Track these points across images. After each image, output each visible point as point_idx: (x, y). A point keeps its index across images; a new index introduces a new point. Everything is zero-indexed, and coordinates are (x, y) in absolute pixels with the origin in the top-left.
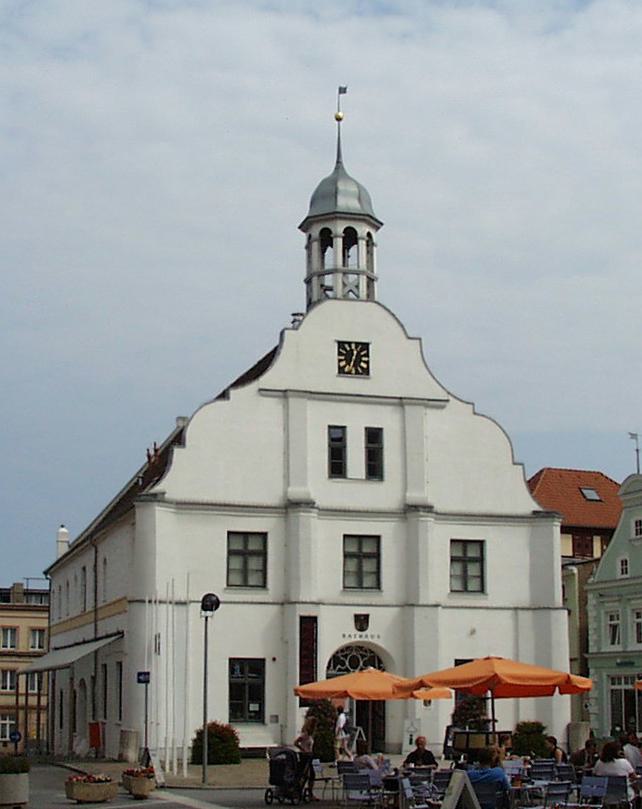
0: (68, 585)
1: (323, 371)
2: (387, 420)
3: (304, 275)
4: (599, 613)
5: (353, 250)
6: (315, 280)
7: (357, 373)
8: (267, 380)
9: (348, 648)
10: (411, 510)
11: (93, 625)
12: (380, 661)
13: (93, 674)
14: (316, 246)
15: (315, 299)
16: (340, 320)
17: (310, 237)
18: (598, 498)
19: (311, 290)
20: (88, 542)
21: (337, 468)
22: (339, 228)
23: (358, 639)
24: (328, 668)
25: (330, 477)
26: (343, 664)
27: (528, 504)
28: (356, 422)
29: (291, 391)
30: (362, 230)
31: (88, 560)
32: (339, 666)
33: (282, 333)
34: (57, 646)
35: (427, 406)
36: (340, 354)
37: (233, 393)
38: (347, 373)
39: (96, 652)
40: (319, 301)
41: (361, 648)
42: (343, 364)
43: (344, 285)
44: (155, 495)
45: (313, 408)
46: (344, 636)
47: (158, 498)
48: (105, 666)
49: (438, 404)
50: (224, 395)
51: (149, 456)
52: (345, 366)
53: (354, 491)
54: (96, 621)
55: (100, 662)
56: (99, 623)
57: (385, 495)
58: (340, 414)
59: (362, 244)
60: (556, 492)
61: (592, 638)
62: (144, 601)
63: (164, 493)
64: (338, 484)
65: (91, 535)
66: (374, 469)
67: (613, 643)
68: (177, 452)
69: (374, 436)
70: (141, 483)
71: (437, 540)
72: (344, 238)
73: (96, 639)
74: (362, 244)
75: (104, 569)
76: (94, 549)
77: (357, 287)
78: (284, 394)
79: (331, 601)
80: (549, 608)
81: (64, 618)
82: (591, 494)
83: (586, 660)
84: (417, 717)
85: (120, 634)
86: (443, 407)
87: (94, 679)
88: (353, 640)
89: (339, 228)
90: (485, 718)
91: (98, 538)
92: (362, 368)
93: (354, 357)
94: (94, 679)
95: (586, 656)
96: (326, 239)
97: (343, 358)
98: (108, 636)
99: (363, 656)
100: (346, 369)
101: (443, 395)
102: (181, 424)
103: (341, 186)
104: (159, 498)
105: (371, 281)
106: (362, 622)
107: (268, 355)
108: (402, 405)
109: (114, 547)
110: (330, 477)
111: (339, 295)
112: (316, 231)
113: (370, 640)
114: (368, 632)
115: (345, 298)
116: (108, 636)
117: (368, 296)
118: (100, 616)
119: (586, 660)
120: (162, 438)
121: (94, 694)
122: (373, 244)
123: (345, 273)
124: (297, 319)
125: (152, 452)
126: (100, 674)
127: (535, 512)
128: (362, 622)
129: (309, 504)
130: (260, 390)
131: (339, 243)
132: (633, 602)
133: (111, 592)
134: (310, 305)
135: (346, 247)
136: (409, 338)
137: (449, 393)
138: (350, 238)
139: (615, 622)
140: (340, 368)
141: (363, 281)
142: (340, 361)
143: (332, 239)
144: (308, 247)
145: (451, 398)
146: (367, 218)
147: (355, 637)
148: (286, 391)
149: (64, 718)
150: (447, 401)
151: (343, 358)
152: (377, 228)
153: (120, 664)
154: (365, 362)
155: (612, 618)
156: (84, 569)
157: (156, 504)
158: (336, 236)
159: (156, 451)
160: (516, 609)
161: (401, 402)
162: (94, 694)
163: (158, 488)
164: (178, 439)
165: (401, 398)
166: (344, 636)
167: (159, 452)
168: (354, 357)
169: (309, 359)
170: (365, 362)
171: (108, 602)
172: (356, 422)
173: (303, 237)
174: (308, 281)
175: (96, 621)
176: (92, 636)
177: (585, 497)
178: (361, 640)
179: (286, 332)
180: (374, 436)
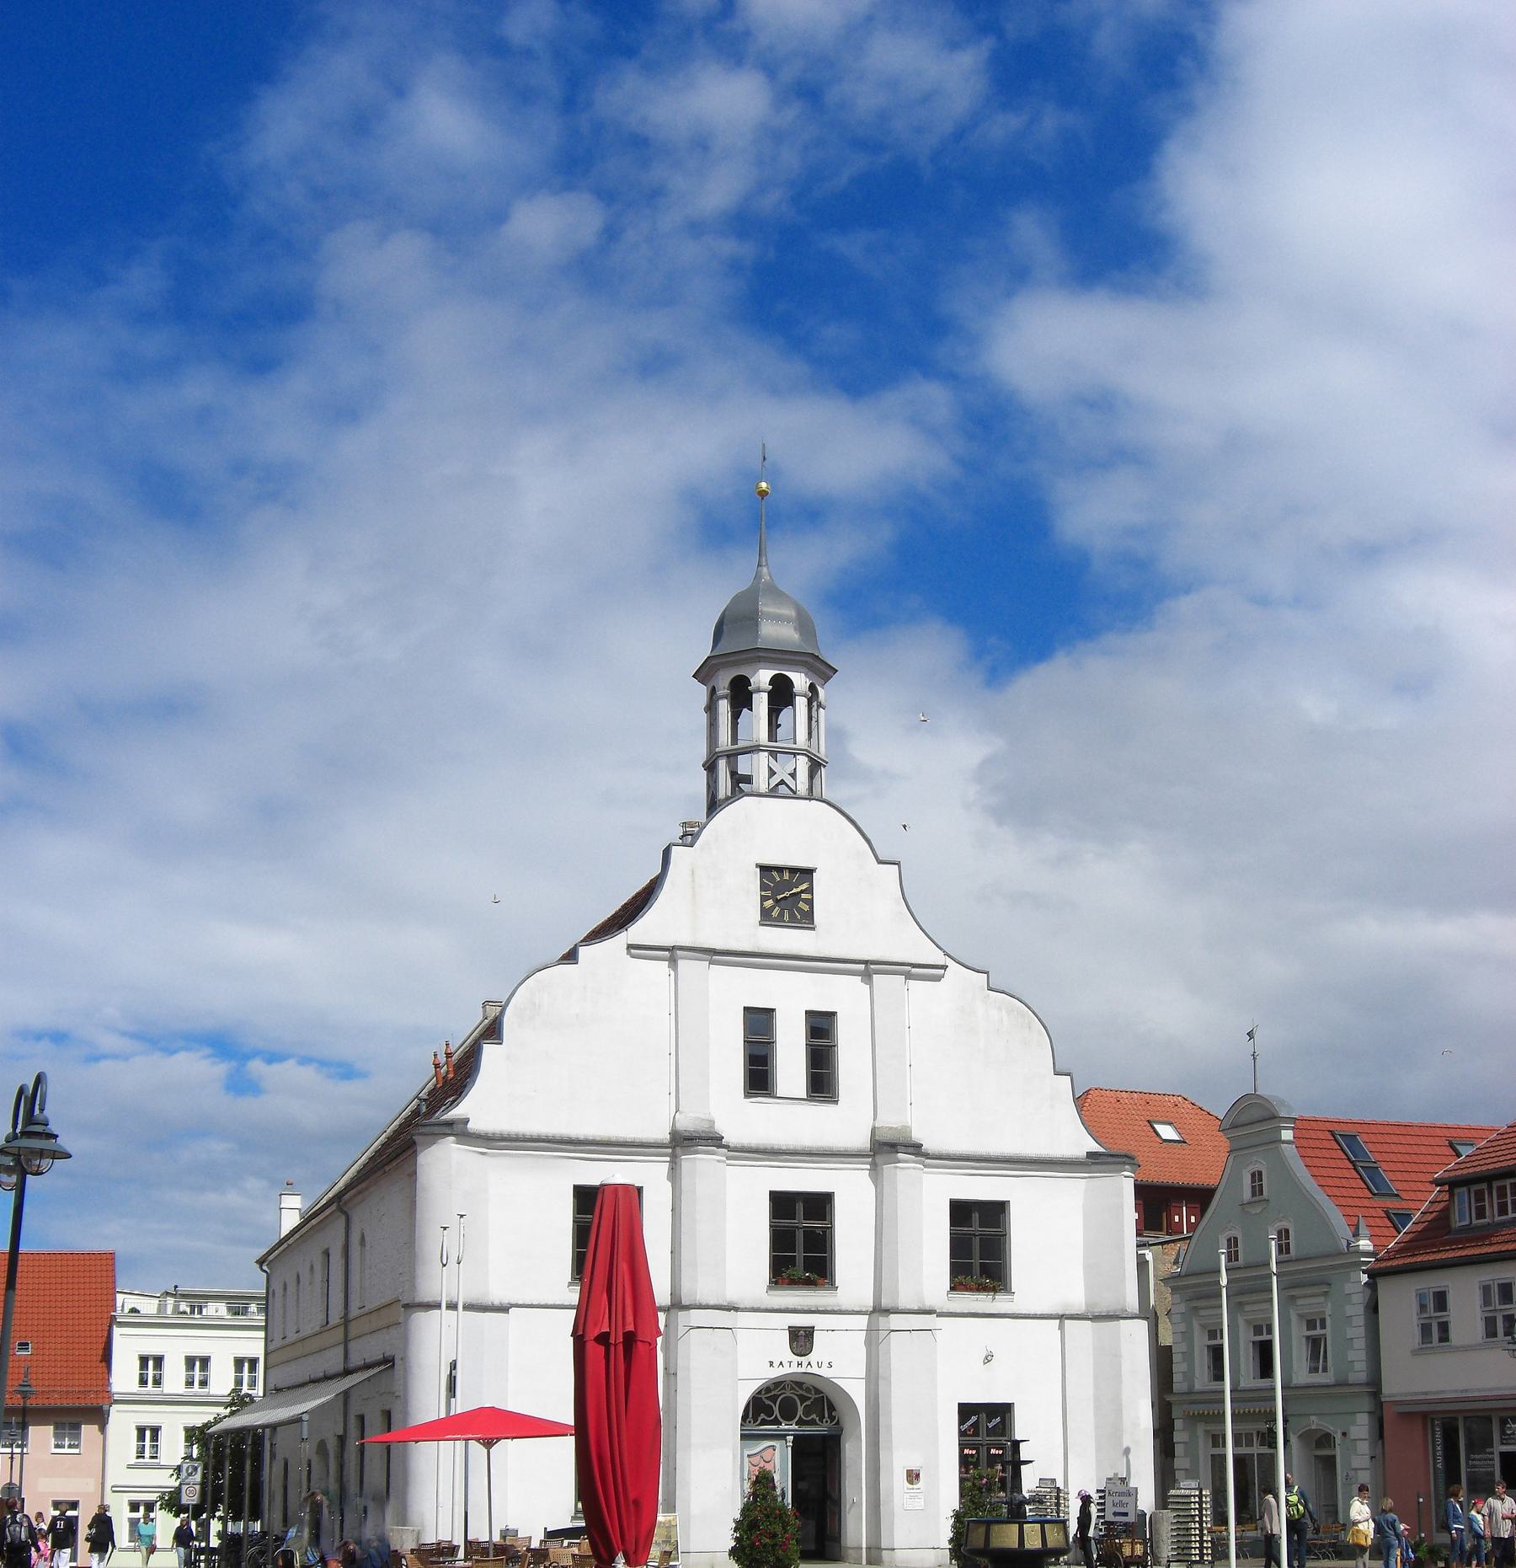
0: (285, 1289)
1: (736, 916)
2: (840, 995)
3: (701, 752)
5: (785, 715)
6: (722, 764)
7: (793, 918)
8: (638, 931)
9: (778, 1384)
10: (887, 1148)
11: (341, 1348)
12: (832, 1408)
13: (341, 1433)
14: (724, 707)
15: (721, 795)
16: (766, 829)
17: (713, 691)
18: (1177, 1138)
19: (716, 781)
20: (334, 1207)
21: (759, 1078)
22: (763, 677)
23: (795, 1369)
24: (744, 1418)
25: (748, 1095)
26: (770, 1412)
27: (1081, 1143)
28: (792, 1000)
29: (682, 948)
30: (800, 681)
31: (333, 1237)
32: (763, 1416)
34: (280, 1386)
35: (909, 976)
36: (763, 887)
38: (775, 920)
39: (346, 1394)
40: (729, 800)
41: (799, 1384)
42: (769, 903)
43: (772, 773)
44: (450, 1124)
45: (721, 975)
46: (771, 1364)
47: (459, 1131)
48: (361, 1418)
49: (929, 972)
50: (571, 957)
51: (437, 1066)
52: (772, 908)
53: (788, 1118)
54: (346, 1341)
55: (354, 1411)
56: (352, 1345)
57: (845, 1122)
58: (762, 988)
59: (801, 703)
60: (1115, 1124)
61: (1178, 1368)
62: (438, 1306)
63: (467, 1121)
64: (760, 1107)
65: (339, 1196)
66: (822, 1081)
67: (1314, 1370)
68: (489, 1051)
69: (820, 1027)
70: (424, 1109)
71: (929, 1198)
72: (770, 693)
73: (347, 1372)
74: (801, 703)
76: (342, 1221)
77: (793, 775)
78: (672, 954)
79: (748, 1306)
80: (1096, 1318)
81: (292, 1337)
82: (1167, 1132)
83: (1169, 1404)
84: (1029, 1481)
86: (938, 979)
87: (342, 1440)
88: (786, 1370)
89: (763, 677)
91: (351, 1199)
92: (800, 910)
93: (786, 892)
94: (342, 1440)
95: (1169, 1398)
96: (741, 696)
97: (769, 893)
98: (367, 1367)
99: (803, 1399)
100: (775, 913)
102: (493, 1012)
105: (815, 766)
106: (801, 1340)
107: (638, 895)
108: (867, 976)
109: (370, 1216)
110: (748, 1095)
111: (763, 788)
112: (723, 681)
113: (815, 1370)
114: (813, 1357)
115: (773, 793)
116: (367, 1367)
118: (352, 1334)
119: (1169, 1404)
120: (462, 1028)
121: (341, 1466)
122: (820, 705)
123: (773, 754)
124: (690, 836)
125: (442, 1059)
126: (353, 1431)
127: (1090, 1155)
128: (801, 1340)
129: (714, 1140)
130: (630, 947)
131: (761, 702)
132: (1300, 1302)
133: (371, 1290)
134: (714, 805)
135: (774, 713)
136: (880, 862)
137: (946, 954)
138: (781, 694)
141: (802, 764)
142: (763, 899)
143: (751, 694)
144: (711, 708)
145: (949, 962)
147: (788, 1364)
148: (672, 949)
150: (945, 967)
151: (769, 893)
152: (826, 679)
153: (388, 1415)
155: (1311, 1325)
156: (327, 1253)
157: (452, 1138)
158: (759, 691)
159: (449, 1055)
160: (1062, 1317)
161: (868, 969)
163: (457, 1112)
165: (866, 962)
166: (771, 1364)
167: (455, 1057)
168: (786, 892)
169: (711, 896)
171: (369, 1307)
172: (792, 1000)
173: (702, 691)
174: (711, 767)
175: (346, 1341)
176: (340, 1367)
177: (1158, 1134)
178: (800, 1370)
180: (820, 1027)
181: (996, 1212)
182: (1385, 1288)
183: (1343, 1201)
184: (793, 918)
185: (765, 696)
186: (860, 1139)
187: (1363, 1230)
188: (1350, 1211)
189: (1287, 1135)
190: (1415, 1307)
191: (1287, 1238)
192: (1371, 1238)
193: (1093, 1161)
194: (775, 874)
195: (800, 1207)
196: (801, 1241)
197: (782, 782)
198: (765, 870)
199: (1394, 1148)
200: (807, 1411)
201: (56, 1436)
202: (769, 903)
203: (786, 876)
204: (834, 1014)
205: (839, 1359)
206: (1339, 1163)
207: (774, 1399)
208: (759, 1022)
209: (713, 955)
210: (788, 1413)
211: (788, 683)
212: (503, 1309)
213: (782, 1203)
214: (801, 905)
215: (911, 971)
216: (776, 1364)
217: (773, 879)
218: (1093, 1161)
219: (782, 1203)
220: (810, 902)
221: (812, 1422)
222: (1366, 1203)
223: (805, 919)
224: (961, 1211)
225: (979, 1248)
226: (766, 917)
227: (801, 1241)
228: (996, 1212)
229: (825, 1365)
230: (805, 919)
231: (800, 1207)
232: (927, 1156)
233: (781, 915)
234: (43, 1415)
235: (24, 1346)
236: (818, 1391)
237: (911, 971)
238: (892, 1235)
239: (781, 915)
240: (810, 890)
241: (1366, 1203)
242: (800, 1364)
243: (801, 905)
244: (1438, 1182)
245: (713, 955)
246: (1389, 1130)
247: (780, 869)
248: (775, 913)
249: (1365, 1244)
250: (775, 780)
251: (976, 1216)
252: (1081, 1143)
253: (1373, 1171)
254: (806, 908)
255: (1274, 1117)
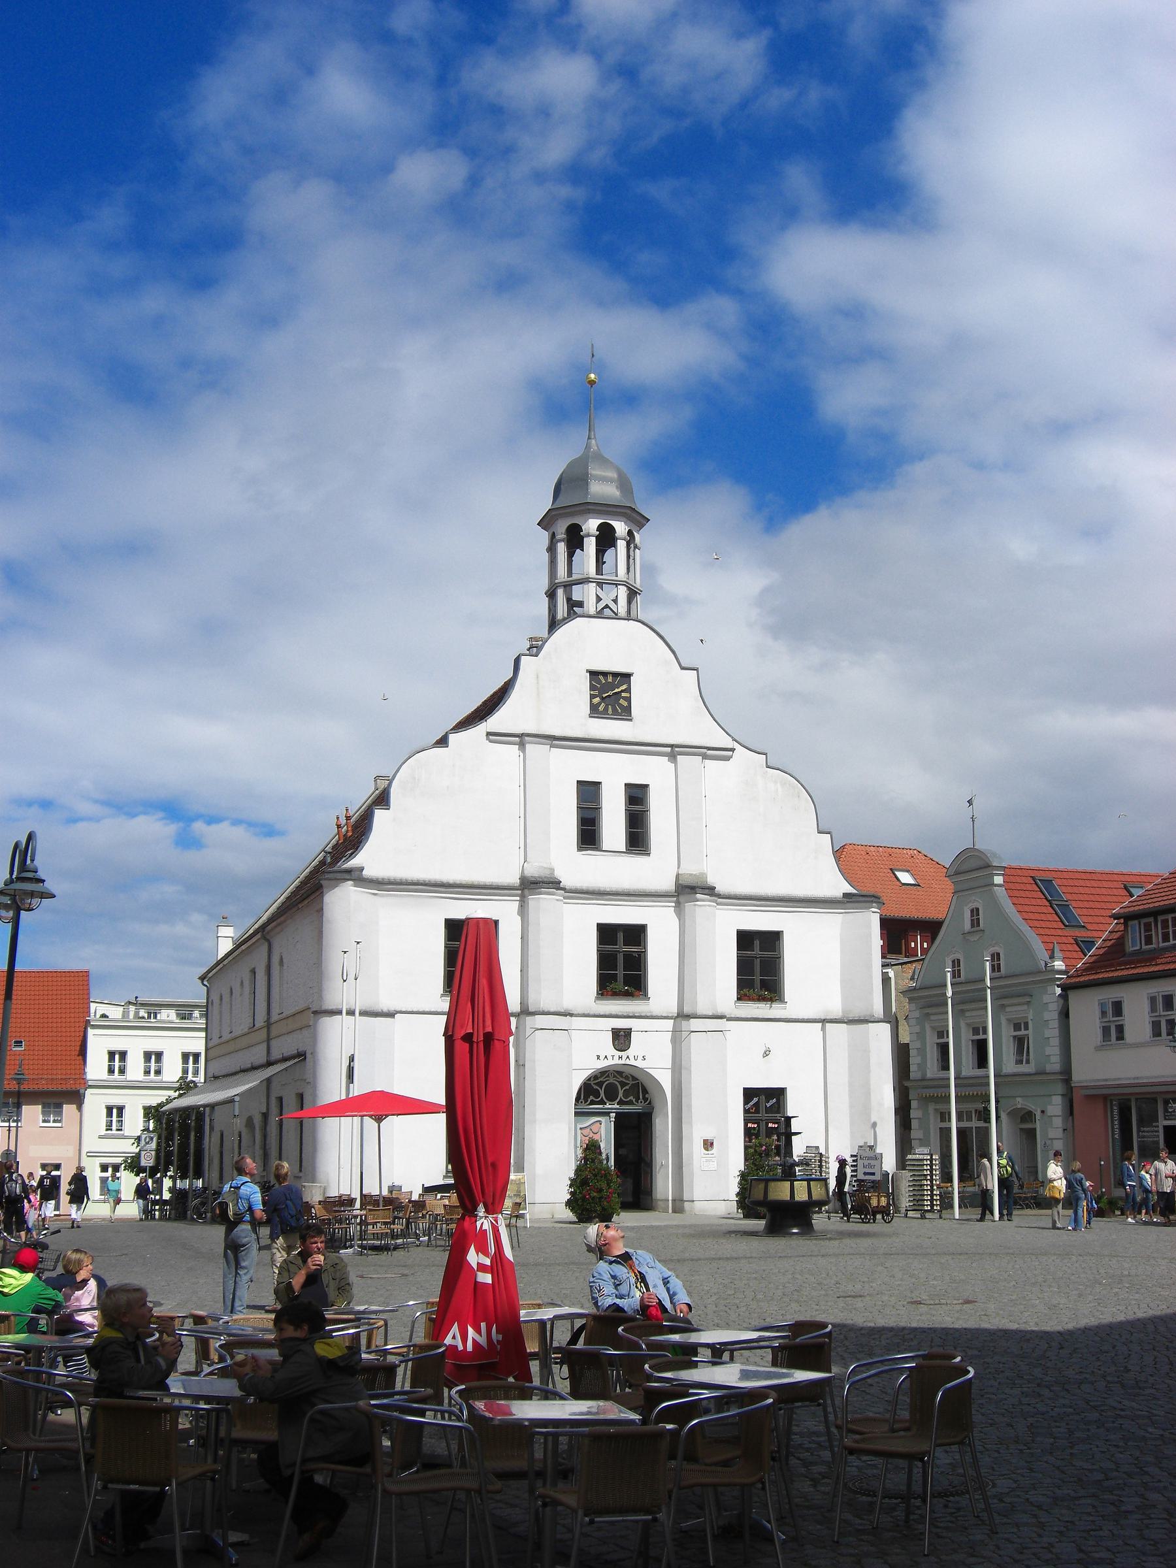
0: (221, 999)
1: (571, 710)
3: (544, 583)
4: (923, 1029)
5: (609, 555)
6: (560, 592)
7: (615, 712)
8: (495, 722)
10: (688, 890)
11: (265, 1045)
12: (645, 1091)
14: (561, 548)
15: (560, 616)
16: (594, 643)
17: (553, 536)
19: (555, 606)
20: (259, 936)
21: (589, 836)
22: (591, 525)
23: (616, 1061)
24: (577, 1099)
25: (580, 849)
26: (597, 1095)
27: (839, 886)
28: (614, 775)
29: (529, 735)
30: (621, 528)
31: (259, 959)
33: (517, 661)
34: (217, 1074)
35: (705, 757)
36: (592, 688)
37: (452, 738)
38: (601, 713)
39: (268, 1081)
40: (565, 620)
41: (620, 1073)
42: (597, 700)
43: (599, 599)
44: (349, 871)
46: (598, 1057)
47: (357, 877)
48: (280, 1099)
49: (721, 754)
50: (443, 742)
51: (339, 826)
52: (599, 704)
53: (611, 867)
54: (268, 1040)
57: (656, 870)
58: (591, 766)
59: (621, 545)
60: (865, 871)
61: (914, 1060)
62: (340, 1012)
63: (362, 869)
64: (590, 858)
66: (637, 838)
67: (1019, 1062)
68: (379, 815)
69: (636, 796)
70: (329, 860)
71: (720, 929)
72: (597, 537)
73: (269, 1064)
74: (621, 545)
75: (281, 972)
76: (265, 947)
77: (615, 601)
78: (521, 739)
80: (850, 1022)
82: (906, 878)
85: (301, 1056)
86: (728, 759)
87: (265, 1116)
88: (610, 1062)
89: (591, 525)
90: (791, 1161)
92: (621, 706)
93: (610, 692)
94: (265, 1116)
95: (906, 1084)
97: (596, 693)
98: (285, 1059)
99: (623, 1084)
100: (601, 708)
101: (727, 742)
102: (382, 784)
103: (594, 470)
104: (355, 875)
105: (632, 594)
106: (621, 1038)
108: (672, 757)
109: (287, 943)
111: (592, 611)
112: (561, 528)
113: (632, 1062)
114: (631, 1052)
115: (600, 615)
116: (285, 1059)
117: (629, 611)
120: (359, 797)
121: (265, 1137)
122: (636, 547)
124: (535, 648)
125: (343, 821)
126: (274, 1109)
127: (846, 895)
128: (621, 1038)
129: (554, 884)
130: (489, 734)
131: (590, 545)
133: (288, 1001)
135: (600, 553)
136: (683, 668)
138: (606, 538)
139: (1023, 1032)
140: (592, 705)
141: (622, 592)
142: (592, 697)
143: (582, 538)
144: (552, 549)
145: (736, 746)
146: (628, 511)
147: (611, 1058)
149: (216, 1161)
150: (733, 750)
151: (596, 693)
152: (641, 526)
154: (625, 698)
155: (1017, 1027)
156: (253, 972)
158: (588, 535)
159: (348, 818)
160: (823, 1021)
161: (673, 751)
162: (265, 1137)
163: (354, 862)
164: (382, 799)
165: (672, 746)
166: (598, 1057)
167: (353, 820)
168: (610, 692)
169: (551, 695)
170: (625, 698)
172: (614, 775)
173: (545, 536)
174: (551, 595)
175: (268, 1040)
176: (263, 1060)
177: (898, 879)
178: (621, 1062)
179: (523, 658)
180: (636, 796)
181: (772, 939)
182: (1074, 998)
183: (1042, 931)
184: (615, 712)
185: (593, 539)
186: (667, 883)
187: (1057, 953)
188: (1046, 939)
189: (998, 880)
190: (1098, 1013)
191: (999, 959)
192: (1064, 959)
193: (848, 901)
194: (601, 677)
195: (620, 936)
196: (621, 962)
197: (607, 606)
198: (594, 674)
199: (1082, 890)
200: (626, 1094)
201: (44, 1113)
202: (597, 700)
203: (610, 679)
204: (647, 786)
205: (651, 1054)
206: (1039, 902)
207: (600, 1084)
208: (589, 793)
209: (553, 740)
210: (611, 1096)
211: (612, 529)
212: (391, 1015)
213: (606, 933)
214: (622, 701)
215: (706, 752)
216: (602, 1057)
217: (599, 682)
218: (848, 901)
219: (606, 933)
220: (629, 700)
221: (630, 1103)
222: (1059, 932)
223: (625, 713)
224: (745, 939)
225: (760, 967)
226: (595, 711)
227: (621, 962)
228: (772, 939)
229: (640, 1058)
230: (625, 713)
231: (620, 936)
232: (719, 896)
233: (606, 709)
234: (34, 1097)
235: (18, 1043)
236: (634, 1078)
237: (706, 752)
238: (692, 958)
239: (606, 709)
240: (628, 690)
241: (1059, 932)
242: (620, 1058)
243: (622, 701)
244: (1115, 917)
245: (553, 740)
246: (1077, 876)
247: (605, 674)
248: (601, 708)
249: (1059, 965)
250: (601, 605)
251: (757, 943)
252: (839, 886)
253: (1065, 908)
254: (625, 704)
255: (988, 866)
